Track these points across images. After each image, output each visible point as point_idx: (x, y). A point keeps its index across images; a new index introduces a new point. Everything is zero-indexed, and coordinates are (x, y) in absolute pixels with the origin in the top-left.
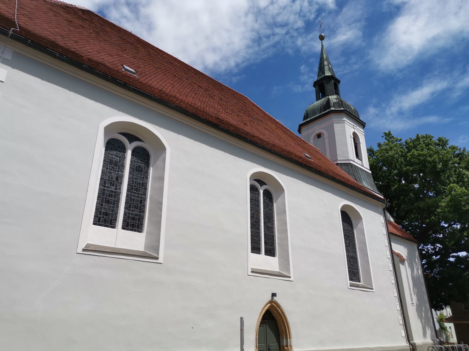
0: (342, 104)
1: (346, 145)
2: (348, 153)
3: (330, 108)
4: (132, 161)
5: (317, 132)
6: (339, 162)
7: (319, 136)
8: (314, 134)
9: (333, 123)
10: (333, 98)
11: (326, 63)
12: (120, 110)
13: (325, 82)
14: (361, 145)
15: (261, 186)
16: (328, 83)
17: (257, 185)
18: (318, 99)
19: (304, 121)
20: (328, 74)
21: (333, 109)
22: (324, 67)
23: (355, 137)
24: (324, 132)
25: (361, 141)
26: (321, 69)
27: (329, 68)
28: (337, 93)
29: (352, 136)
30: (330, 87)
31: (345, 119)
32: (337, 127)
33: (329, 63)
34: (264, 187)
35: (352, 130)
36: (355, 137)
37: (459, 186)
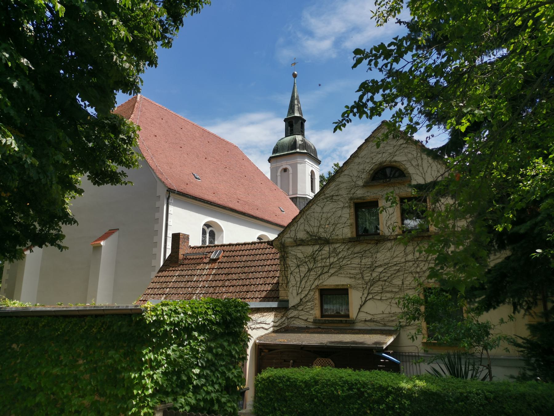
0: (305, 146)
1: (305, 183)
2: (306, 189)
3: (296, 148)
4: (209, 239)
5: (284, 167)
6: (298, 196)
7: (285, 170)
8: (281, 168)
9: (297, 163)
10: (299, 138)
11: (296, 102)
12: (206, 215)
13: (294, 121)
14: (316, 180)
15: (208, 228)
16: (296, 123)
17: (206, 228)
18: (287, 136)
19: (274, 155)
20: (297, 114)
21: (298, 150)
22: (294, 106)
23: (312, 173)
24: (289, 167)
25: (316, 177)
26: (292, 108)
27: (298, 108)
28: (302, 133)
29: (310, 174)
30: (297, 126)
31: (306, 160)
32: (300, 167)
33: (299, 102)
34: (210, 229)
35: (311, 169)
36: (312, 173)
37: (545, 126)
